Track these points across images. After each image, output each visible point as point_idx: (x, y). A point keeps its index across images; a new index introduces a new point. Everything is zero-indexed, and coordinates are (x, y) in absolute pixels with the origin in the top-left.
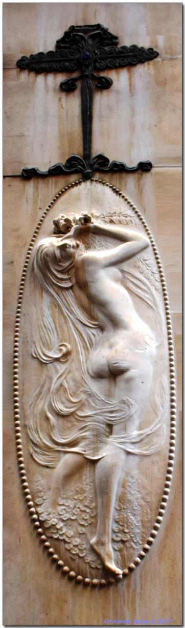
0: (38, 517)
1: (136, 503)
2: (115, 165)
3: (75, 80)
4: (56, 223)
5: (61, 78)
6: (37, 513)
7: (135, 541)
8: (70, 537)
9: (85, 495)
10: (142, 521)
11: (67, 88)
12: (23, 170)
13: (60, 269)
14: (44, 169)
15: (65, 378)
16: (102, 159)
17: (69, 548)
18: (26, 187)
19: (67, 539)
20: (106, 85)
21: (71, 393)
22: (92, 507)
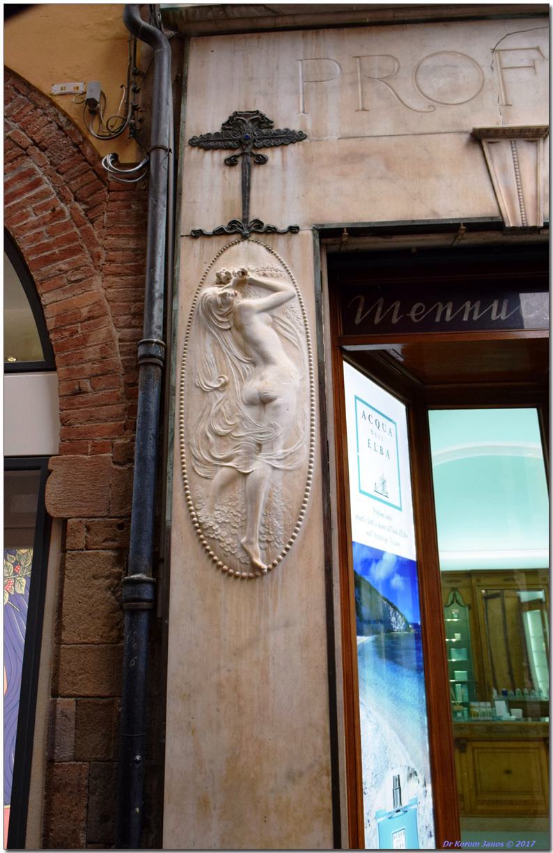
2: (269, 228)
3: (236, 157)
4: (218, 276)
5: (226, 154)
6: (197, 516)
10: (284, 525)
11: (230, 163)
13: (221, 313)
14: (209, 230)
16: (258, 223)
19: (221, 539)
20: (262, 161)
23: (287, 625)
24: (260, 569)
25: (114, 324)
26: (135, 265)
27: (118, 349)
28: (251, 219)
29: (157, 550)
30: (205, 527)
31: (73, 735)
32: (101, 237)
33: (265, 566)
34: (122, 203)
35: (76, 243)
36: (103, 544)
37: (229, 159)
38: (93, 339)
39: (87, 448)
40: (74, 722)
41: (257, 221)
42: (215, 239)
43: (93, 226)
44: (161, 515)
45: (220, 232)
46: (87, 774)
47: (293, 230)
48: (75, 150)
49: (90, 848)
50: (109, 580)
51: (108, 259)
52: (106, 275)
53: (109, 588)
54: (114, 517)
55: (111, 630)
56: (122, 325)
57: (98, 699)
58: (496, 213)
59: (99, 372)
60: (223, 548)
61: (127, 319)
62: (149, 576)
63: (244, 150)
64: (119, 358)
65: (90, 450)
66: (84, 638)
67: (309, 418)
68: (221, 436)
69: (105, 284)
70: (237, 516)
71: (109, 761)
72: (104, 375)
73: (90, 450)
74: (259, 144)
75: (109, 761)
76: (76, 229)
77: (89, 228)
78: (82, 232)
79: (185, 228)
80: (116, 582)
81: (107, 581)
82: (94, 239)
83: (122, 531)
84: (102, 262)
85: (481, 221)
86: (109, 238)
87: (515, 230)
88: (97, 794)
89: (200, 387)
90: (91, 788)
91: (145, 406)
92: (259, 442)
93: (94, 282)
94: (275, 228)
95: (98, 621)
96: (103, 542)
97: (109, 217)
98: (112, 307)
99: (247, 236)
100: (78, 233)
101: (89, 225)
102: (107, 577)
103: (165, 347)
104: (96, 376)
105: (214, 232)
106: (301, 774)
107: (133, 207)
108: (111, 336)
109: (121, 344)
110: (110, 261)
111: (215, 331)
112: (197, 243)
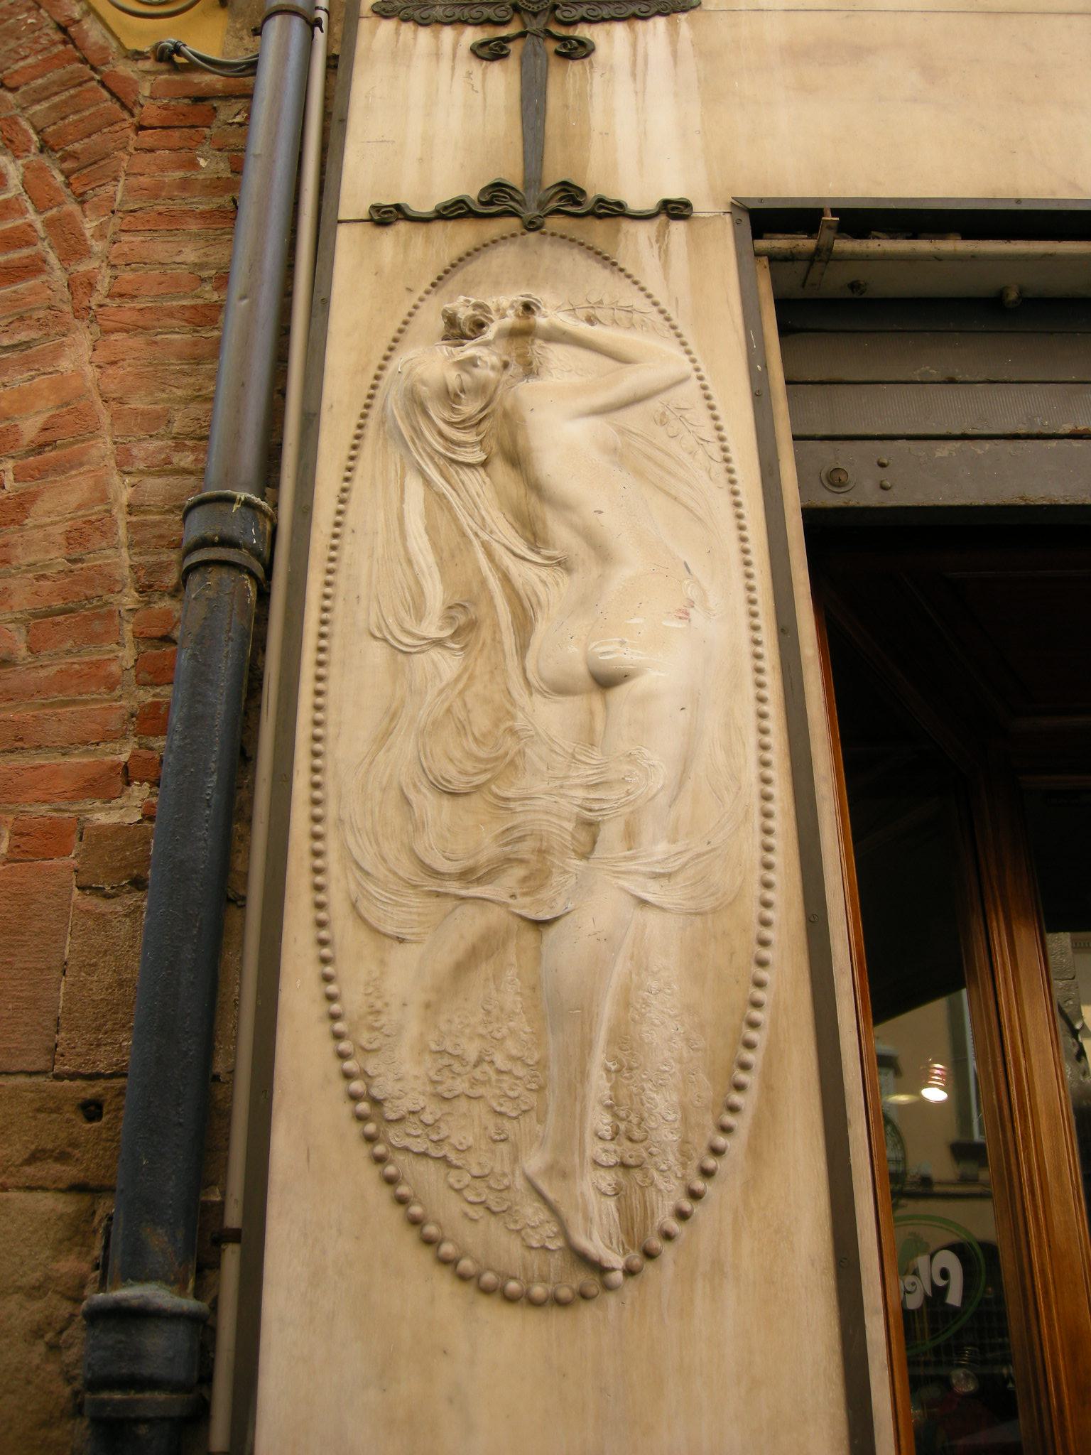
0: (368, 1086)
1: (667, 1054)
2: (601, 201)
3: (507, 40)
4: (451, 321)
5: (472, 35)
6: (364, 1075)
7: (664, 1167)
8: (463, 1151)
9: (512, 1024)
10: (684, 1108)
11: (491, 52)
12: (373, 207)
13: (457, 418)
14: (427, 208)
15: (461, 693)
16: (570, 194)
17: (457, 1186)
18: (544, 938)
19: (452, 1157)
20: (578, 51)
21: (477, 734)
22: (531, 1062)
24: (599, 1269)
25: (119, 464)
26: (194, 307)
27: (122, 532)
29: (216, 1198)
30: (392, 1116)
32: (103, 236)
33: (616, 1260)
34: (173, 155)
35: (26, 252)
36: (29, 1170)
37: (483, 44)
38: (41, 511)
41: (565, 186)
42: (438, 226)
43: (83, 211)
44: (232, 1072)
45: (456, 211)
47: (675, 210)
48: (58, 36)
49: (226, 1180)
50: (39, 1304)
51: (114, 290)
53: (37, 1333)
54: (73, 1076)
56: (142, 466)
59: (58, 604)
60: (458, 1191)
61: (161, 450)
62: (182, 1292)
63: (525, 25)
64: (122, 560)
67: (752, 738)
68: (454, 794)
69: (101, 356)
70: (509, 1072)
72: (72, 611)
74: (566, 14)
76: (32, 216)
77: (70, 215)
78: (49, 224)
80: (65, 1308)
83: (95, 1124)
84: (96, 299)
86: (125, 237)
89: (385, 640)
92: (588, 815)
94: (620, 204)
96: (31, 1160)
97: (129, 190)
98: (115, 417)
99: (538, 222)
100: (39, 226)
101: (72, 207)
103: (271, 519)
104: (46, 616)
105: (437, 211)
107: (202, 163)
108: (104, 499)
109: (134, 519)
110: (121, 296)
111: (437, 466)
112: (390, 240)
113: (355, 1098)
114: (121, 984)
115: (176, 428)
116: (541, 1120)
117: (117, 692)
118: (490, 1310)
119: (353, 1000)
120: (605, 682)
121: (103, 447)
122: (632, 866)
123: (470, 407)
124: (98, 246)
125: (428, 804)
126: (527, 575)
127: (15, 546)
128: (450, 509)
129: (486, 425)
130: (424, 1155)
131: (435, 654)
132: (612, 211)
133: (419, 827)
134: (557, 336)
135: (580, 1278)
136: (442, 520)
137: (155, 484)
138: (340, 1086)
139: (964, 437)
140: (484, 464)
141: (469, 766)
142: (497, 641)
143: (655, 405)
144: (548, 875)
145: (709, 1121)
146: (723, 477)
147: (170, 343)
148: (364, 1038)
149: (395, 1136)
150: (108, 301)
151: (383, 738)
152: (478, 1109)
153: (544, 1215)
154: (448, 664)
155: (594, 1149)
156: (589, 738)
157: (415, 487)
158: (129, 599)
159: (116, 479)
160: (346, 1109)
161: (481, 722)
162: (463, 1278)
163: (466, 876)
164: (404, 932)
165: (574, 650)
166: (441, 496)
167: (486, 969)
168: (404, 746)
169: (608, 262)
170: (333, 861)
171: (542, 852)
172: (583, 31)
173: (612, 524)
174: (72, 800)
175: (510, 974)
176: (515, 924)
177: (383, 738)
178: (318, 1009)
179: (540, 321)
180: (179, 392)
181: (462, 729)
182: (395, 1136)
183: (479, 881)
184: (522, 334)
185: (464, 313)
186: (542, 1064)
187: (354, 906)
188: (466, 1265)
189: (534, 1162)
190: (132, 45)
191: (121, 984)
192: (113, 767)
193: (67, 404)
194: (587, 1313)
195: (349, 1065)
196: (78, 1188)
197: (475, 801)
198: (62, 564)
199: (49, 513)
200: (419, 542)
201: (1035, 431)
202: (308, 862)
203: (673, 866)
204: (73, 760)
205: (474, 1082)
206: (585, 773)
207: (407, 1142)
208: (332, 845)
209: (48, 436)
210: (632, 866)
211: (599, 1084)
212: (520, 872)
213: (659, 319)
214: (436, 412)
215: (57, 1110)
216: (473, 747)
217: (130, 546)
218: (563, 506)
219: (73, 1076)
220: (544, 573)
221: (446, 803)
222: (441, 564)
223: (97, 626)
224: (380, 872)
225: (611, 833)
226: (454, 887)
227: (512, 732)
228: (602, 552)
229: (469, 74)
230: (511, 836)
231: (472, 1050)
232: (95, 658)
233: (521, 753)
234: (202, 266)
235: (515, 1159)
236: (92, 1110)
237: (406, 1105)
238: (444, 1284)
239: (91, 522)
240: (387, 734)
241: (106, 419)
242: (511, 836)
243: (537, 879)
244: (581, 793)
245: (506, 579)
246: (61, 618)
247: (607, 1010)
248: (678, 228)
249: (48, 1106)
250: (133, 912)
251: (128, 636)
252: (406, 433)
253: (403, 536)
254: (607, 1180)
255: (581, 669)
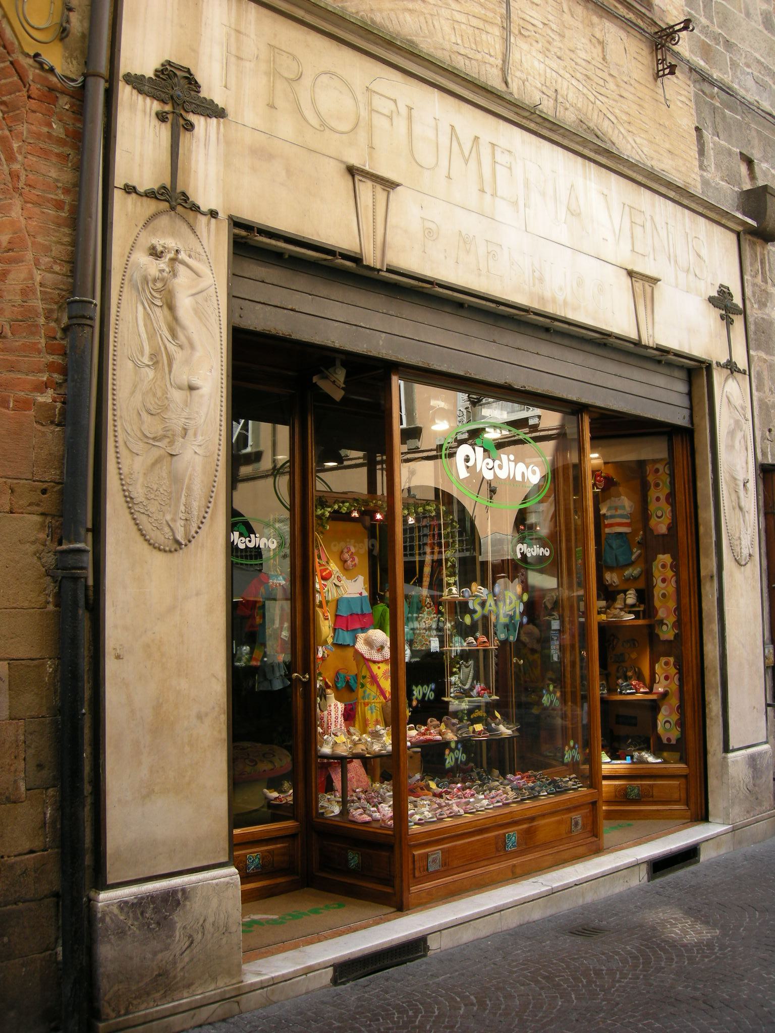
5: (156, 106)
6: (128, 490)
23: (197, 594)
24: (180, 544)
26: (56, 200)
28: (178, 190)
31: (8, 696)
33: (183, 543)
36: (29, 508)
39: (8, 402)
40: (7, 683)
42: (145, 199)
46: (23, 730)
47: (213, 214)
52: (26, 202)
54: (38, 481)
55: (39, 596)
57: (30, 661)
58: (358, 251)
63: (174, 108)
64: (38, 304)
65: (11, 405)
66: (13, 603)
71: (43, 717)
73: (11, 406)
75: (43, 717)
79: (119, 179)
81: (33, 547)
82: (13, 153)
85: (348, 253)
86: (29, 157)
87: (369, 268)
88: (33, 746)
90: (27, 743)
91: (693, 561)
93: (14, 207)
95: (25, 586)
96: (28, 506)
102: (33, 543)
106: (207, 714)
113: (126, 496)
114: (50, 454)
115: (53, 254)
116: (170, 507)
117: (41, 355)
118: (156, 553)
119: (125, 470)
120: (192, 388)
121: (29, 256)
122: (195, 443)
123: (159, 285)
124: (20, 158)
125: (144, 415)
126: (172, 348)
127: (4, 291)
128: (151, 320)
129: (163, 292)
130: (143, 513)
131: (147, 369)
132: (195, 208)
133: (143, 422)
134: (183, 263)
135: (176, 546)
136: (148, 322)
137: (49, 276)
138: (122, 493)
139: (264, 303)
140: (161, 306)
141: (156, 407)
142: (163, 369)
143: (204, 294)
144: (174, 442)
145: (203, 510)
146: (218, 322)
147: (49, 214)
148: (128, 480)
149: (136, 508)
150: (25, 187)
151: (133, 393)
152: (156, 503)
153: (169, 530)
154: (150, 373)
155: (181, 515)
156: (186, 404)
157: (140, 308)
158: (42, 321)
159: (35, 271)
160: (124, 499)
161: (159, 394)
162: (150, 544)
163: (154, 439)
164: (139, 452)
165: (185, 377)
166: (149, 314)
167: (159, 466)
168: (138, 397)
169: (192, 229)
170: (119, 428)
171: (174, 435)
172: (192, 118)
173: (195, 338)
174: (31, 392)
175: (165, 467)
176: (166, 454)
177: (133, 393)
178: (116, 471)
179: (180, 257)
180: (54, 238)
181: (154, 395)
182: (136, 508)
183: (157, 441)
184: (173, 260)
185: (159, 249)
186: (171, 493)
187: (125, 443)
188: (152, 541)
189: (168, 517)
190: (27, 50)
191: (50, 454)
192: (43, 382)
193: (16, 233)
194: (176, 554)
195: (125, 488)
196: (42, 514)
197: (157, 417)
198: (20, 302)
199: (14, 280)
200: (142, 329)
201: (282, 306)
202: (112, 428)
203: (201, 443)
204: (29, 377)
205: (156, 496)
206: (185, 414)
207: (139, 509)
208: (118, 423)
209: (11, 246)
210: (195, 443)
211: (183, 499)
212: (168, 440)
213: (205, 258)
214: (150, 284)
215: (35, 491)
216: (157, 401)
217: (42, 300)
218: (183, 328)
219: (38, 481)
220: (176, 348)
221: (149, 416)
222: (148, 338)
223: (33, 329)
224: (132, 434)
225: (190, 432)
226: (151, 441)
227: (167, 398)
228: (192, 346)
229: (155, 126)
230: (166, 429)
231: (155, 487)
232: (34, 341)
233: (169, 405)
234: (57, 181)
235: (164, 516)
236: (44, 491)
237: (139, 500)
238: (146, 545)
239: (28, 287)
240: (134, 392)
241: (30, 244)
242: (166, 429)
243: (172, 443)
244: (183, 420)
245: (166, 348)
246: (21, 323)
247: (187, 481)
248: (213, 220)
249: (33, 490)
250: (53, 432)
251: (43, 335)
252: (140, 289)
253: (137, 325)
254: (182, 523)
255: (186, 383)
